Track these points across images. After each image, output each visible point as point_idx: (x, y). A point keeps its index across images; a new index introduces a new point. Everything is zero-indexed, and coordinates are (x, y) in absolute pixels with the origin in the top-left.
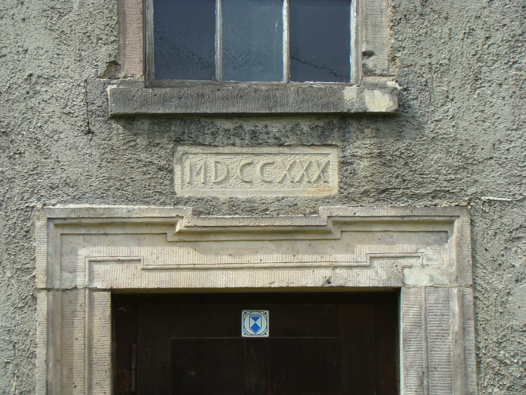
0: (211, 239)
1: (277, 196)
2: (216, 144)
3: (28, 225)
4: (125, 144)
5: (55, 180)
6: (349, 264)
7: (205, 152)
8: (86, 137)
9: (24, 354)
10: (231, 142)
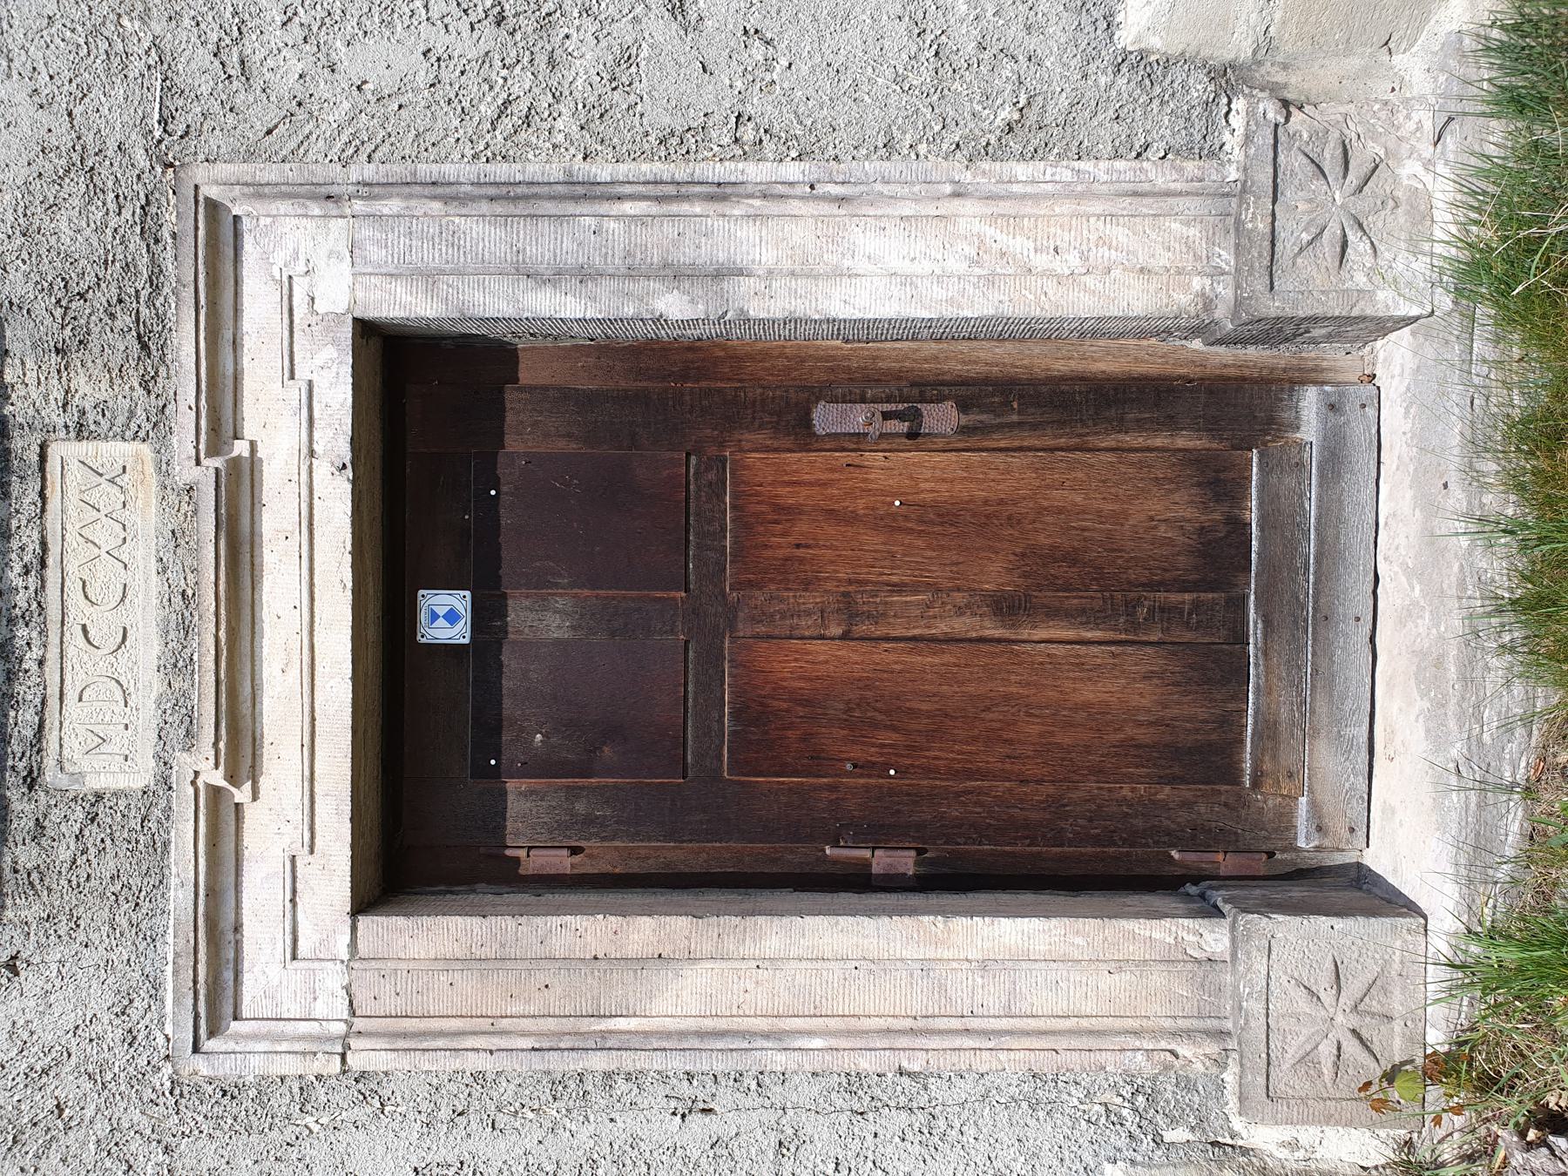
0: (249, 712)
1: (154, 572)
2: (38, 701)
3: (210, 1089)
4: (36, 894)
5: (114, 1035)
6: (305, 424)
7: (57, 723)
8: (22, 973)
9: (476, 1094)
10: (34, 667)
